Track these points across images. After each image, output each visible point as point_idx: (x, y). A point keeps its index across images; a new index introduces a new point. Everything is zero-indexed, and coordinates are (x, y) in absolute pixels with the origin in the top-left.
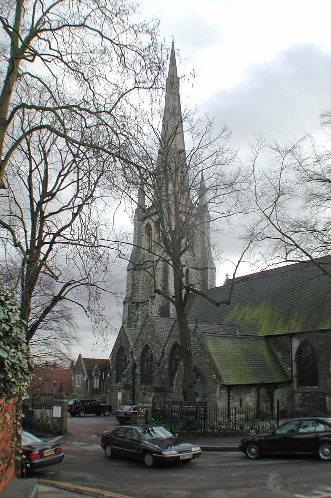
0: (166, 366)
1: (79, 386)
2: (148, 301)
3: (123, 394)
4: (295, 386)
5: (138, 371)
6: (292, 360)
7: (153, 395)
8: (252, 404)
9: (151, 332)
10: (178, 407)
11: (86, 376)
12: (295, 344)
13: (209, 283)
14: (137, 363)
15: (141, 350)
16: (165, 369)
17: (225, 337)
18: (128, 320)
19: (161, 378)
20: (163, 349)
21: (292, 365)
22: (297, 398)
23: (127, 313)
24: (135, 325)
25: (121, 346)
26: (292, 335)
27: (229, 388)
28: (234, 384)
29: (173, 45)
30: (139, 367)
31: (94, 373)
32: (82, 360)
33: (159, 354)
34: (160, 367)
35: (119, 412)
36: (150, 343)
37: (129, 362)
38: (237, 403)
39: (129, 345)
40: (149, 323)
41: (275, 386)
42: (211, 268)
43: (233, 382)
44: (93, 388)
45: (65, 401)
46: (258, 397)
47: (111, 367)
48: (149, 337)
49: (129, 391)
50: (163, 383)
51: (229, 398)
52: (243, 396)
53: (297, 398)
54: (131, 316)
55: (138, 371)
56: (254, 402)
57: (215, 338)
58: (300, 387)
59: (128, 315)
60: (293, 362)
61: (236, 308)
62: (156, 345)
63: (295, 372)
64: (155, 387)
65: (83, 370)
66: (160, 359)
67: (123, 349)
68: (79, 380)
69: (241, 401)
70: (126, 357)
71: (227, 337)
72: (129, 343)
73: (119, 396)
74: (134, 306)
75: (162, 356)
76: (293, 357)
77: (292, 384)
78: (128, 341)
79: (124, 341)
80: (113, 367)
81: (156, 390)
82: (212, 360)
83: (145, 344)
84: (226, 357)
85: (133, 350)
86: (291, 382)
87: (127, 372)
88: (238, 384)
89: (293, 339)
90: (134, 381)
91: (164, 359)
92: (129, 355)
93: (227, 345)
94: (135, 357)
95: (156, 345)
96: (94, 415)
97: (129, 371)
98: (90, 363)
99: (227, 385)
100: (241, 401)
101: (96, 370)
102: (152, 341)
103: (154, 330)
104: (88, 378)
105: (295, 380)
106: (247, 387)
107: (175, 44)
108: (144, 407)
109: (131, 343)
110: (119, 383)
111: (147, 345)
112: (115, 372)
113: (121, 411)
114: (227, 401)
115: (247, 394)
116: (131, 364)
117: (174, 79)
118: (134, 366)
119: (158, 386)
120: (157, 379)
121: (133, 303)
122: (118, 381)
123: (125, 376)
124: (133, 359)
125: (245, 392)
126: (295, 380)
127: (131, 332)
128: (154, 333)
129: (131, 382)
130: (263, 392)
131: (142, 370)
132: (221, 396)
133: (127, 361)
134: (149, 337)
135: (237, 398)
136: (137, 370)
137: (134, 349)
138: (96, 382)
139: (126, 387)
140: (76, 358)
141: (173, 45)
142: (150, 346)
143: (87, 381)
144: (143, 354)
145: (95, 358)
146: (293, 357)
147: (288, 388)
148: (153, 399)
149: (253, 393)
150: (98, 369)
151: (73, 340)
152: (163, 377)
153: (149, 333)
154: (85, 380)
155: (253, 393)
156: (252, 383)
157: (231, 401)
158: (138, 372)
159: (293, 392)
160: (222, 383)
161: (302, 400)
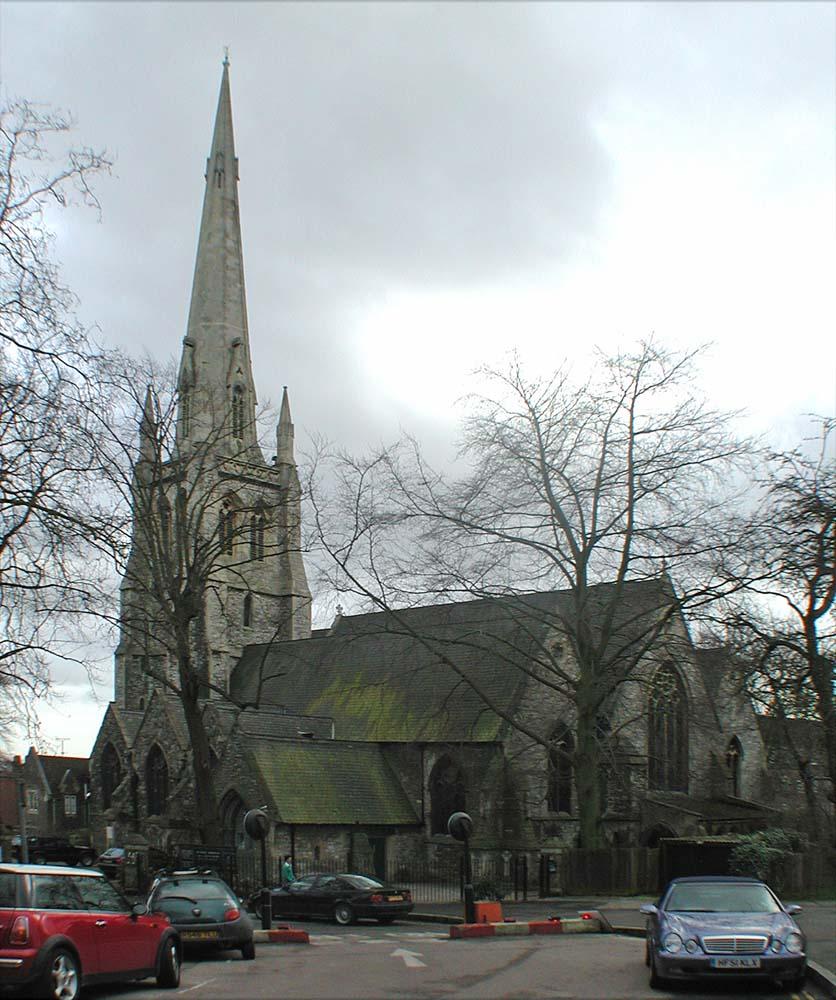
0: (191, 785)
1: (34, 811)
2: (165, 655)
3: (116, 830)
4: (429, 832)
5: (142, 789)
6: (423, 788)
7: (168, 832)
8: (341, 857)
9: (163, 723)
10: (190, 852)
11: (48, 791)
12: (430, 763)
13: (294, 626)
14: (140, 777)
15: (146, 754)
16: (189, 791)
17: (293, 742)
18: (126, 690)
19: (182, 805)
20: (186, 756)
21: (423, 795)
22: (431, 854)
23: (123, 675)
24: (142, 699)
25: (110, 744)
26: (422, 746)
27: (293, 829)
28: (302, 822)
29: (226, 73)
30: (143, 783)
31: (65, 786)
32: (39, 763)
33: (178, 764)
34: (180, 785)
35: (103, 859)
36: (161, 743)
37: (125, 774)
38: (310, 853)
39: (124, 743)
40: (158, 707)
41: (390, 829)
42: (298, 596)
43: (300, 818)
44: (64, 815)
45: (7, 838)
46: (351, 845)
47: (93, 780)
48: (160, 732)
49: (128, 825)
50: (188, 814)
51: (293, 843)
52: (321, 844)
53: (431, 854)
54: (131, 682)
55: (142, 789)
56: (345, 854)
57: (273, 744)
58: (437, 835)
59: (127, 679)
60: (425, 792)
61: (335, 686)
62: (173, 746)
63: (428, 808)
64: (171, 820)
65: (40, 778)
66: (180, 772)
67: (114, 749)
68: (35, 801)
69: (317, 851)
70: (118, 764)
71: (296, 742)
72: (123, 739)
73: (110, 832)
74: (136, 662)
75: (183, 768)
76: (426, 783)
77: (423, 829)
78: (122, 735)
79: (115, 734)
80: (96, 781)
81: (173, 824)
82: (262, 781)
83: (152, 744)
84: (288, 778)
85: (131, 754)
86: (422, 825)
87: (122, 790)
88: (310, 822)
89: (427, 753)
90: (135, 807)
91: (188, 772)
92: (126, 762)
93: (295, 757)
94: (136, 766)
95: (173, 746)
96: (64, 864)
97: (126, 789)
98: (56, 766)
99: (286, 824)
100: (317, 851)
101: (69, 781)
102: (165, 739)
103: (168, 720)
104: (53, 796)
105: (428, 822)
106: (330, 830)
107: (229, 69)
108: (136, 851)
109: (126, 739)
110: (108, 810)
111: (156, 745)
112: (100, 789)
113: (107, 857)
114: (290, 849)
115: (330, 839)
116: (128, 777)
117: (224, 164)
118: (135, 781)
119: (178, 819)
120: (174, 805)
121: (135, 657)
122: (107, 806)
123: (117, 798)
124: (132, 768)
125: (325, 835)
126: (428, 822)
127: (127, 718)
128: (168, 726)
129: (131, 809)
130: (362, 838)
131: (149, 789)
132: (278, 840)
133: (122, 772)
134: (160, 732)
135: (309, 845)
136: (141, 787)
137: (133, 751)
138: (70, 806)
139: (122, 818)
140: (23, 754)
141: (226, 73)
142: (162, 747)
143: (50, 802)
144: (150, 761)
145: (65, 755)
146: (426, 783)
147: (416, 835)
148: (169, 839)
149: (342, 839)
150: (74, 778)
151: (13, 723)
152: (186, 802)
153: (160, 725)
154: (46, 799)
155: (342, 839)
156: (339, 822)
157: (296, 849)
158: (143, 792)
159: (424, 844)
160: (278, 820)
161: (438, 855)
